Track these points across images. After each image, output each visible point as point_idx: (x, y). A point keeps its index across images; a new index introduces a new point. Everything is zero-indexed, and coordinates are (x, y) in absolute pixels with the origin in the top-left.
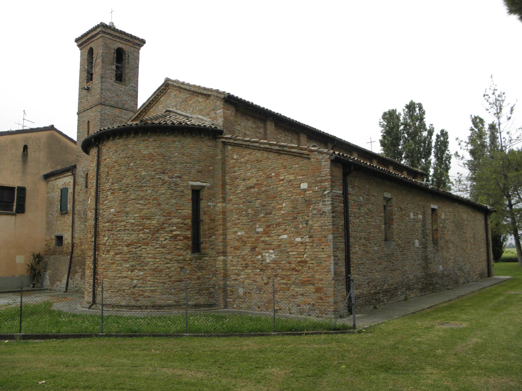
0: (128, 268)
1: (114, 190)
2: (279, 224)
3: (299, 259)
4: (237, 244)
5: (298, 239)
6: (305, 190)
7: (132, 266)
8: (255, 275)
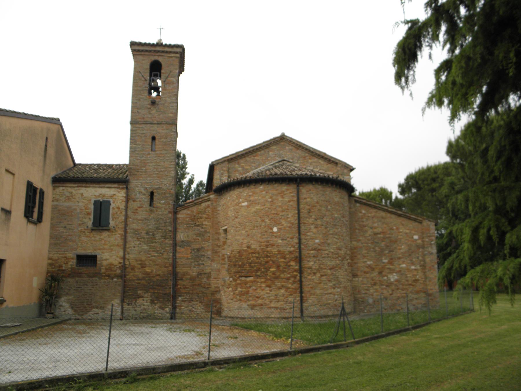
0: (331, 286)
1: (317, 225)
2: (399, 258)
3: (414, 279)
4: (367, 270)
5: (413, 267)
6: (416, 240)
7: (334, 285)
8: (382, 289)
